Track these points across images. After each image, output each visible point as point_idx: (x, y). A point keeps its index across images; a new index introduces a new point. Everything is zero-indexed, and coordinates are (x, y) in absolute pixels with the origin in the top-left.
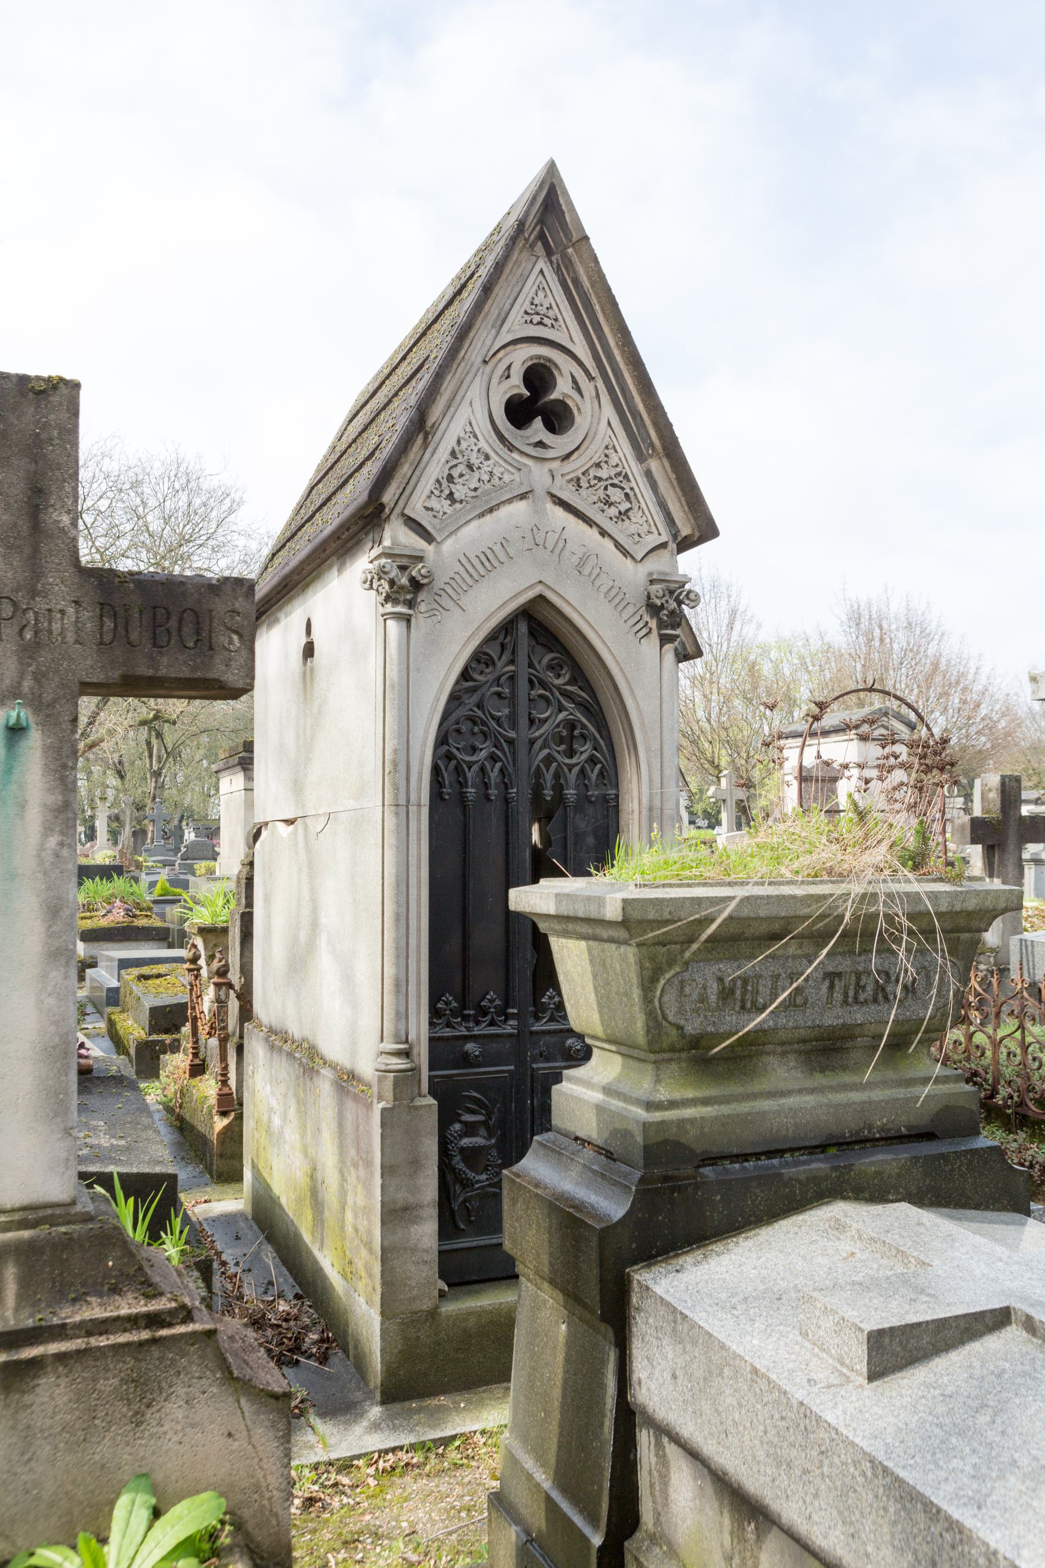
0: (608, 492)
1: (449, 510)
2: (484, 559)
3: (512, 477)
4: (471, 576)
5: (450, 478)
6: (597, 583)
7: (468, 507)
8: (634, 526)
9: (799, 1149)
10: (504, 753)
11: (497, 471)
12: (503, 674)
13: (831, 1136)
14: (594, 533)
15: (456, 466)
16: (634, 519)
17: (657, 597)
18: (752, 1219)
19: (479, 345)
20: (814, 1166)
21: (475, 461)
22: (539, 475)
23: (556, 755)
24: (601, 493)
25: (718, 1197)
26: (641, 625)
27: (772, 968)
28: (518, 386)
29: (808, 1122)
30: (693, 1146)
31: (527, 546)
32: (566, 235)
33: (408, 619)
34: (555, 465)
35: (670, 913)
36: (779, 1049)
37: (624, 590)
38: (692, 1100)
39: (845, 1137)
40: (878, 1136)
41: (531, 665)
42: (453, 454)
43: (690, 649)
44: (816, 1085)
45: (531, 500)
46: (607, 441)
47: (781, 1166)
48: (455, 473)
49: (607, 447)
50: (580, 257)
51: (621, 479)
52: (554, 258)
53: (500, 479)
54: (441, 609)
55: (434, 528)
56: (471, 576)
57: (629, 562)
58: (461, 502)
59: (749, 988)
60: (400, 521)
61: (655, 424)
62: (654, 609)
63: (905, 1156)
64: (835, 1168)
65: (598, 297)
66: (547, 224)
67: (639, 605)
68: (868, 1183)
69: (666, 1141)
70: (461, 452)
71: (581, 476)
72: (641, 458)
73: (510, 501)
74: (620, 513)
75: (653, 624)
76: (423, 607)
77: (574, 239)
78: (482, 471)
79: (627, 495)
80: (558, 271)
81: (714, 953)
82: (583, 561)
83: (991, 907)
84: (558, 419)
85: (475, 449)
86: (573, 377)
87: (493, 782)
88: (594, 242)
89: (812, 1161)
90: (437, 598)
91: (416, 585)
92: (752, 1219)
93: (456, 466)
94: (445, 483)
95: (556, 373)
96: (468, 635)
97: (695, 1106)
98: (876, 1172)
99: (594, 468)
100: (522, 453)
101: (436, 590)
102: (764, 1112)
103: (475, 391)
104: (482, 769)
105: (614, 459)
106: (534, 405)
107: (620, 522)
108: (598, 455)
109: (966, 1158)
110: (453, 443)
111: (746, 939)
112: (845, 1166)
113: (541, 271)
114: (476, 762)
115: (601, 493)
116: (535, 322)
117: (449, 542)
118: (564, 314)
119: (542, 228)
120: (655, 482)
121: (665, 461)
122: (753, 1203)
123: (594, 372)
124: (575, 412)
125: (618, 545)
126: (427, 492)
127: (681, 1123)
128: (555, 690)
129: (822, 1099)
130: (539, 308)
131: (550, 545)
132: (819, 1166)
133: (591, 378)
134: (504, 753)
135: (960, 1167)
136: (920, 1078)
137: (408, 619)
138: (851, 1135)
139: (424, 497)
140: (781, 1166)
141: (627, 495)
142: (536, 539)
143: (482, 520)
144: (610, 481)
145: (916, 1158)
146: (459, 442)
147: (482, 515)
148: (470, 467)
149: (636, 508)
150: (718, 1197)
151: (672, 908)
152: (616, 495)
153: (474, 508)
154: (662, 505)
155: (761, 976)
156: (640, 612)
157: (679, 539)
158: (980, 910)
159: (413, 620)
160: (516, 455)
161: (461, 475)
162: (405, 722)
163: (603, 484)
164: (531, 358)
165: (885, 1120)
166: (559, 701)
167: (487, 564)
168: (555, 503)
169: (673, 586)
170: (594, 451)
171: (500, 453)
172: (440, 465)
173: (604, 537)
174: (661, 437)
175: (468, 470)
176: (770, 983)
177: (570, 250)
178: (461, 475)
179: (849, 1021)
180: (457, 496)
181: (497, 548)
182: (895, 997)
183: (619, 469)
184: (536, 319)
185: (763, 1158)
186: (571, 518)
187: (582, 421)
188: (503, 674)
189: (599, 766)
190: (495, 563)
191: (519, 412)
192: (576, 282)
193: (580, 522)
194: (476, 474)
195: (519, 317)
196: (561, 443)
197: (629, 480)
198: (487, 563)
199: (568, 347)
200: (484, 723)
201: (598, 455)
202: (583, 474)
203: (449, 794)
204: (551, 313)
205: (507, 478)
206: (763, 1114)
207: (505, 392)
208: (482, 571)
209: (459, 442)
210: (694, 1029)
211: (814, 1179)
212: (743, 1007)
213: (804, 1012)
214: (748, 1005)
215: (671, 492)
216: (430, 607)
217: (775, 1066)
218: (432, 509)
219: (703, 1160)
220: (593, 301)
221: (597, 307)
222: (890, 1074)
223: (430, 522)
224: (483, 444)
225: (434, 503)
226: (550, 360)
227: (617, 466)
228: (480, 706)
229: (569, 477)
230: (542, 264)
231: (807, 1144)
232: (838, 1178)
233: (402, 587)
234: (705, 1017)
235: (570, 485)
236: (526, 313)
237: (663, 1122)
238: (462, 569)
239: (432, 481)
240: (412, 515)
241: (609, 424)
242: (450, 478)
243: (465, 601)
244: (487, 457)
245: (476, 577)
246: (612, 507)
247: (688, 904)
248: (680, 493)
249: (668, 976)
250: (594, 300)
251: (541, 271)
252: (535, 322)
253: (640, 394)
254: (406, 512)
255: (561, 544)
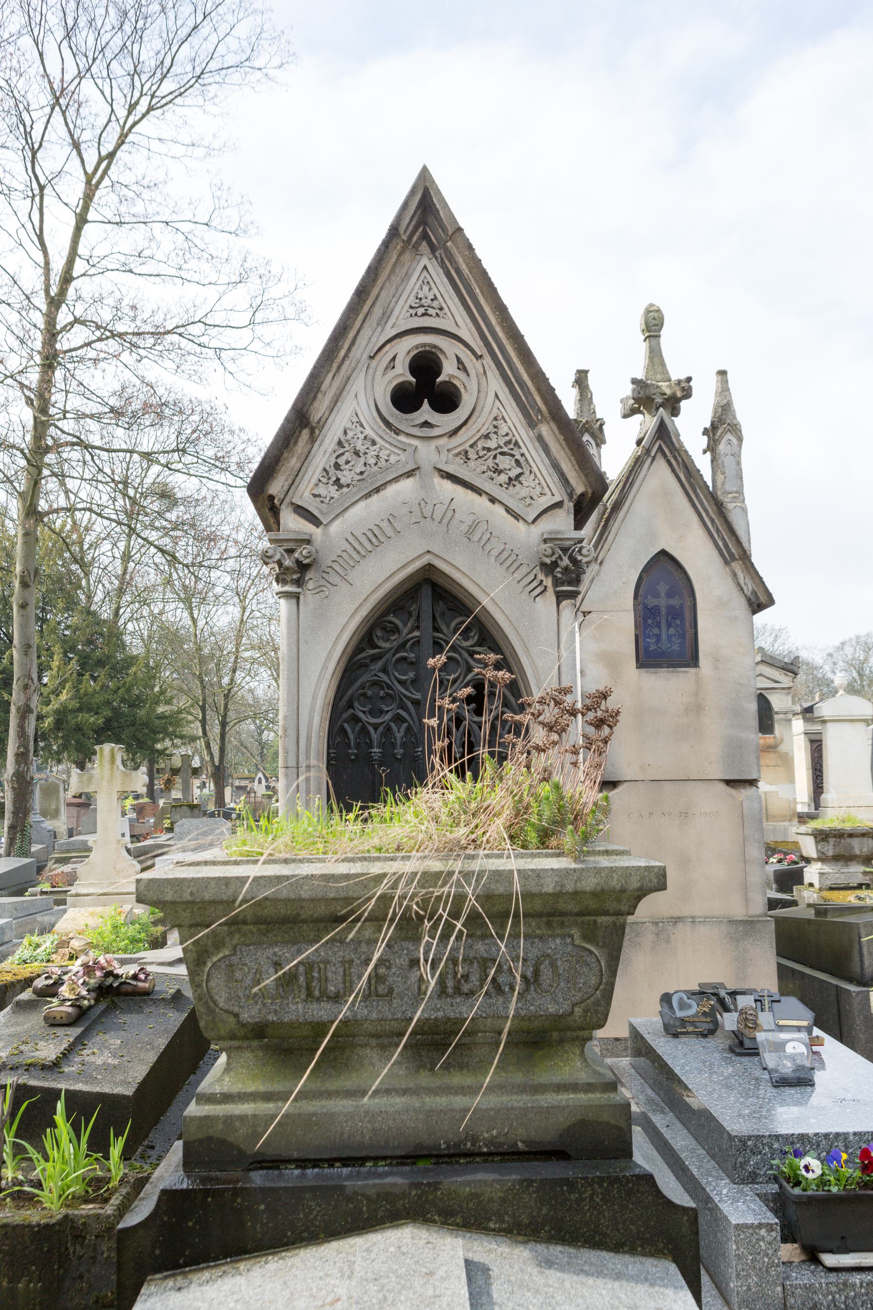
0: (497, 461)
1: (336, 494)
2: (371, 536)
3: (398, 458)
4: (358, 552)
5: (337, 466)
6: (488, 547)
7: (354, 489)
8: (526, 489)
9: (384, 1158)
10: (410, 714)
11: (383, 455)
12: (408, 640)
13: (420, 1146)
14: (484, 501)
15: (343, 454)
16: (525, 484)
17: (547, 556)
18: (305, 1235)
19: (364, 343)
20: (389, 1180)
21: (360, 447)
22: (428, 454)
23: (361, 715)
24: (490, 463)
25: (262, 1207)
26: (535, 584)
27: (341, 953)
28: (403, 375)
29: (390, 1128)
30: (241, 1146)
31: (414, 520)
32: (443, 231)
33: (297, 597)
34: (443, 441)
35: (191, 894)
36: (374, 1042)
37: (516, 551)
38: (251, 1094)
39: (440, 1149)
40: (485, 1150)
41: (436, 629)
42: (340, 443)
43: (763, 599)
44: (411, 1085)
45: (417, 477)
46: (495, 412)
47: (349, 1177)
48: (341, 461)
49: (496, 419)
50: (457, 248)
51: (511, 446)
52: (437, 254)
53: (387, 461)
54: (328, 585)
55: (321, 512)
56: (358, 552)
57: (521, 525)
58: (348, 486)
59: (316, 974)
60: (290, 509)
61: (539, 390)
62: (549, 568)
63: (514, 1177)
64: (417, 1185)
65: (477, 281)
66: (424, 224)
67: (532, 566)
68: (460, 1206)
69: (210, 1139)
70: (347, 441)
71: (468, 448)
72: (532, 424)
73: (396, 480)
74: (510, 479)
75: (548, 582)
76: (311, 585)
77: (450, 233)
78: (368, 456)
79: (517, 461)
80: (442, 265)
81: (270, 935)
82: (473, 527)
83: (618, 887)
84: (446, 400)
85: (362, 436)
86: (458, 359)
87: (398, 742)
88: (468, 233)
89: (391, 1174)
90: (324, 575)
91: (303, 567)
92: (305, 1235)
93: (343, 454)
94: (332, 471)
95: (442, 357)
96: (355, 607)
97: (254, 1101)
98: (471, 1194)
99: (483, 440)
100: (408, 435)
101: (324, 567)
102: (333, 1114)
103: (358, 384)
104: (388, 729)
105: (504, 430)
106: (425, 388)
107: (511, 488)
108: (485, 427)
109: (601, 1186)
110: (339, 434)
111: (304, 921)
112: (428, 1184)
113: (425, 267)
114: (381, 724)
115: (490, 463)
116: (419, 314)
117: (337, 524)
118: (449, 302)
119: (424, 229)
120: (547, 445)
121: (552, 424)
122: (306, 1216)
123: (480, 349)
124: (462, 390)
125: (508, 510)
126: (314, 480)
127: (229, 1120)
128: (463, 652)
129: (415, 1102)
130: (423, 301)
131: (438, 516)
132: (396, 1180)
133: (479, 357)
134: (410, 714)
135: (591, 1197)
136: (552, 1084)
137: (297, 597)
138: (448, 1147)
139: (311, 485)
140: (349, 1177)
141: (517, 461)
142: (423, 513)
143: (369, 500)
144: (500, 450)
145: (530, 1182)
146: (345, 433)
147: (368, 495)
148: (357, 453)
149: (528, 473)
150: (262, 1207)
151: (194, 889)
152: (505, 462)
153: (360, 490)
154: (556, 466)
155: (327, 962)
156: (534, 572)
157: (575, 497)
158: (603, 890)
159: (301, 597)
160: (402, 438)
161: (347, 462)
162: (295, 691)
163: (493, 453)
164: (417, 347)
165: (494, 1132)
166: (467, 662)
167: (374, 540)
168: (442, 477)
169: (567, 544)
170: (482, 423)
171: (385, 437)
172: (327, 455)
173: (494, 503)
174: (545, 402)
175: (354, 457)
176: (341, 970)
177: (449, 244)
178: (347, 462)
179: (452, 1015)
180: (343, 481)
181: (385, 525)
182: (512, 989)
183: (507, 438)
184: (421, 311)
185: (337, 1164)
186: (460, 490)
187: (467, 401)
188: (408, 640)
189: (405, 725)
190: (382, 539)
191: (405, 399)
192: (458, 271)
193: (469, 492)
194: (362, 460)
195: (404, 312)
196: (447, 421)
197: (520, 447)
198: (375, 538)
199: (453, 331)
200: (389, 687)
201: (485, 427)
202: (471, 446)
203: (354, 754)
204: (435, 304)
205: (393, 459)
206: (331, 1116)
207: (390, 382)
208: (369, 547)
209: (345, 433)
210: (253, 1017)
211: (386, 1196)
212: (310, 995)
213: (390, 1003)
214: (317, 993)
215: (563, 453)
216: (318, 584)
217: (374, 1061)
218: (319, 496)
219: (252, 1164)
220: (474, 286)
221: (477, 291)
222: (518, 1077)
223: (317, 508)
224: (368, 431)
225: (321, 490)
226: (435, 347)
227: (507, 435)
228: (384, 670)
229: (457, 451)
230: (425, 261)
231: (389, 1153)
232: (420, 1197)
233: (288, 568)
234: (264, 1004)
235: (458, 459)
236: (411, 307)
237: (206, 1117)
238: (348, 546)
239: (319, 470)
240: (300, 503)
241: (497, 396)
242: (337, 466)
243: (352, 576)
244: (374, 443)
245: (363, 553)
246: (502, 475)
247: (213, 884)
248: (570, 454)
249: (215, 959)
250: (474, 285)
251: (425, 267)
252: (419, 314)
253: (523, 364)
254: (294, 501)
255: (449, 515)
